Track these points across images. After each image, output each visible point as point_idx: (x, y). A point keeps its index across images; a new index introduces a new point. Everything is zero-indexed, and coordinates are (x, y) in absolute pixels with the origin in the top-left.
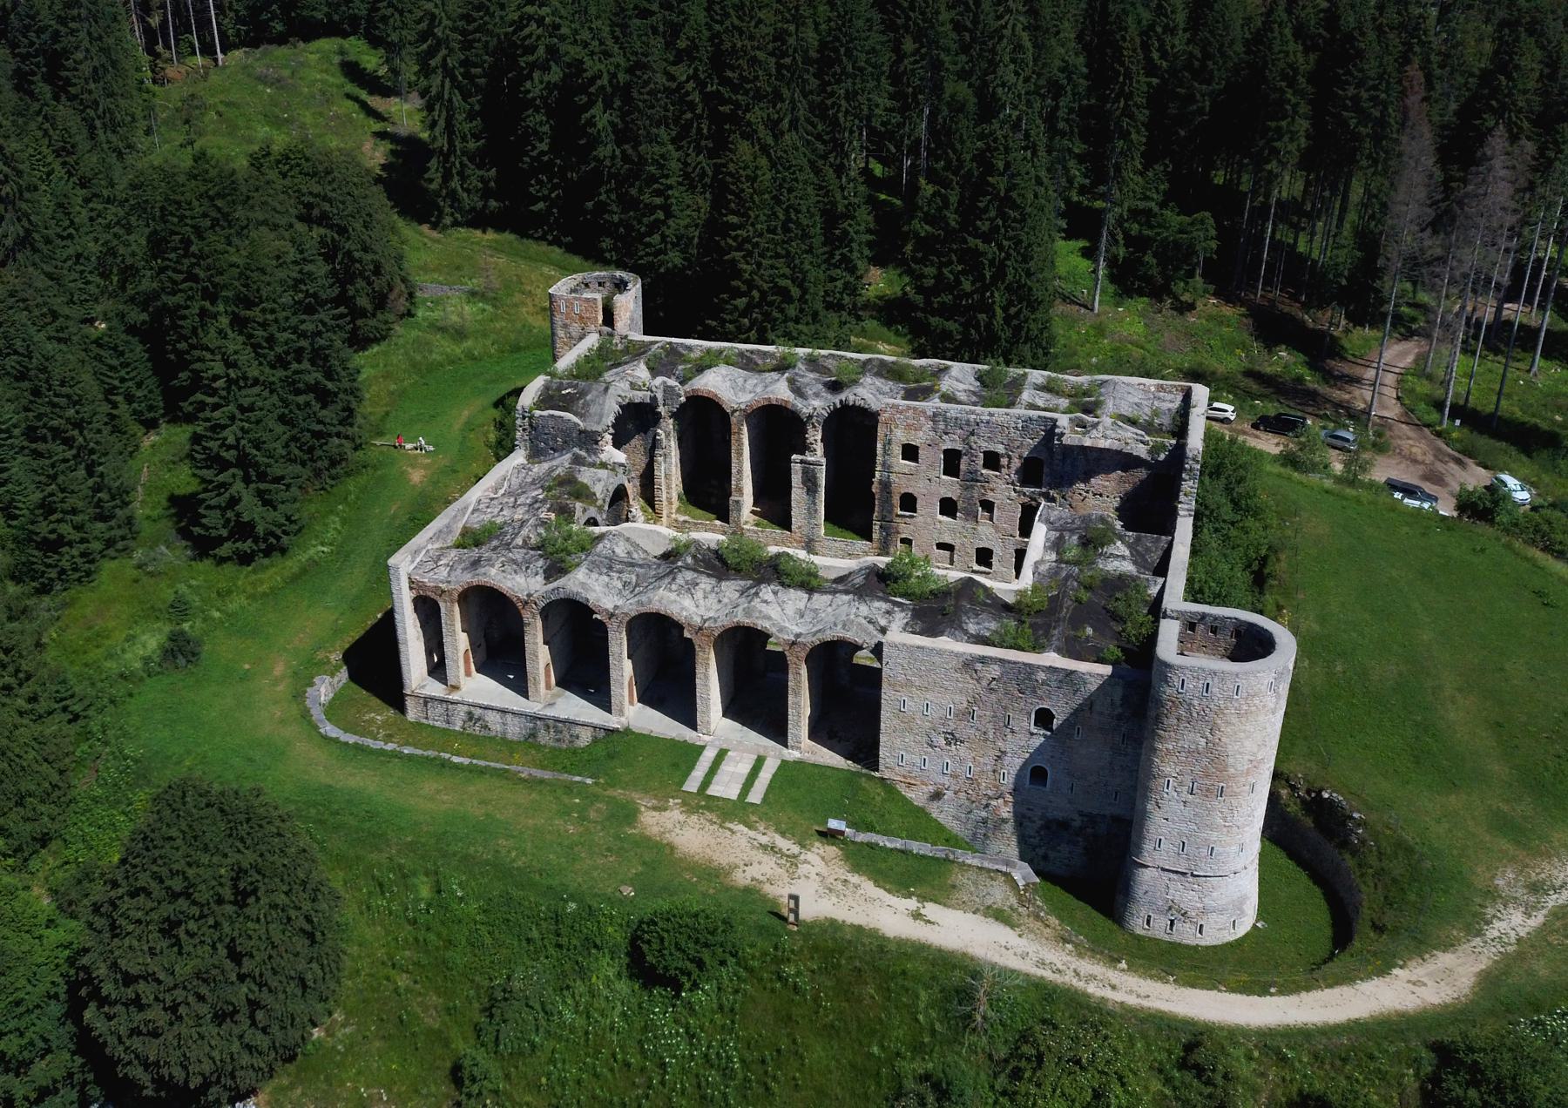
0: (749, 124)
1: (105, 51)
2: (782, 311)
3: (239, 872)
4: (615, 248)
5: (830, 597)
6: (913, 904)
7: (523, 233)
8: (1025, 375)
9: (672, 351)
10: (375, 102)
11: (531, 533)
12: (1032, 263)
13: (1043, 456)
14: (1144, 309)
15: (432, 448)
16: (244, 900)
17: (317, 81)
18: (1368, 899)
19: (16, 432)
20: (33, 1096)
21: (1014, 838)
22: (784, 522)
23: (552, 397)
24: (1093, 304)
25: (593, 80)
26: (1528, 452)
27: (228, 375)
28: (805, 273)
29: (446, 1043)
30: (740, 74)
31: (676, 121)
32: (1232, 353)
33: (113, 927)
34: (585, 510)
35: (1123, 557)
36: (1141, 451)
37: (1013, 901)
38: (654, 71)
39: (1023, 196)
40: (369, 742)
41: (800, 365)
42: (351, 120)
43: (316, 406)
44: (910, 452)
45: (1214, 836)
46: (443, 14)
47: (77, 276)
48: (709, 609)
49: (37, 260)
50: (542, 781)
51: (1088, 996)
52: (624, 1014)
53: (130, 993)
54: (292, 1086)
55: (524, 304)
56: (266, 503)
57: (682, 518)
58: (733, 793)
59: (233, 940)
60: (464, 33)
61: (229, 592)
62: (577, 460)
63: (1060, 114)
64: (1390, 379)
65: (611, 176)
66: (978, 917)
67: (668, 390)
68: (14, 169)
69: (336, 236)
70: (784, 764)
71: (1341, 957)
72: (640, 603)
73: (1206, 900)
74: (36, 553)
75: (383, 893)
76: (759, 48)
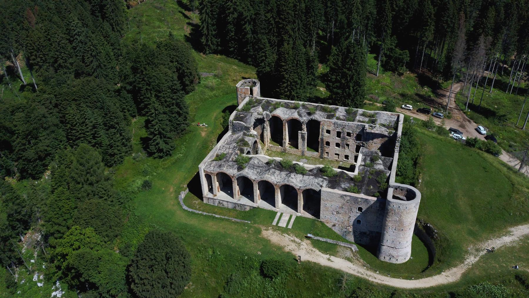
0: (287, 30)
1: (115, 5)
2: (296, 87)
3: (167, 253)
4: (252, 61)
6: (328, 256)
8: (357, 110)
9: (268, 102)
10: (186, 13)
11: (234, 157)
13: (362, 134)
18: (437, 252)
19: (101, 124)
22: (297, 147)
23: (237, 117)
25: (246, 18)
26: (487, 117)
28: (301, 77)
29: (217, 291)
32: (412, 88)
33: (137, 266)
35: (381, 164)
36: (386, 134)
37: (352, 255)
38: (262, 15)
42: (180, 19)
43: (177, 116)
44: (328, 132)
47: (112, 72)
50: (238, 222)
51: (369, 281)
52: (259, 284)
53: (142, 282)
55: (229, 79)
56: (166, 143)
57: (271, 145)
61: (158, 167)
62: (245, 134)
63: (369, 25)
64: (453, 95)
65: (250, 42)
66: (344, 260)
67: (267, 115)
70: (297, 218)
71: (430, 268)
72: (261, 178)
73: (398, 254)
74: (108, 157)
76: (289, 10)
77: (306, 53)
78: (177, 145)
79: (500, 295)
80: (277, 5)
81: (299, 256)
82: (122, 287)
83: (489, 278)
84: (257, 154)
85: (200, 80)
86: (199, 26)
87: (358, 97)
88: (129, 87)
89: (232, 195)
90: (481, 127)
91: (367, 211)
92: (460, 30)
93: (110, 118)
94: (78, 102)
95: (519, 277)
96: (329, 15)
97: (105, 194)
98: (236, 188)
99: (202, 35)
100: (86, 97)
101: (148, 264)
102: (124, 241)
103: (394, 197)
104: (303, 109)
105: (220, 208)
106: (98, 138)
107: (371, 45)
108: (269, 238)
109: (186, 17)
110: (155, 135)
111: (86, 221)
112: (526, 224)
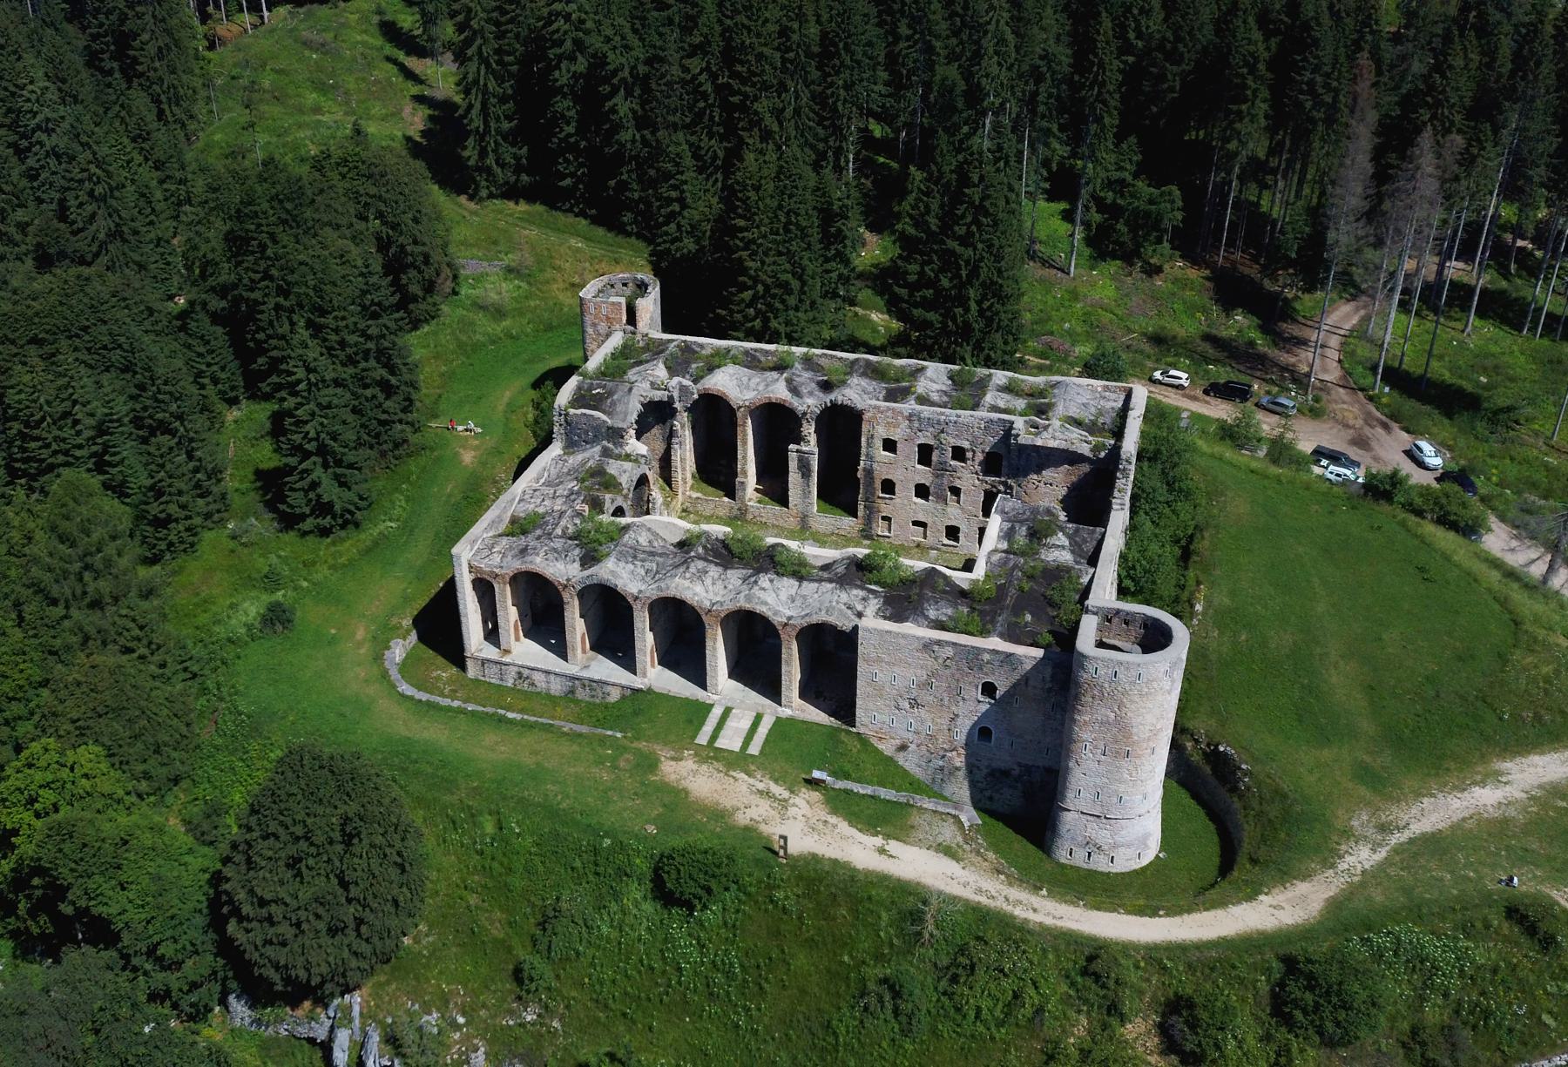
0: (756, 113)
1: (168, 32)
2: (783, 302)
3: (346, 820)
4: (635, 222)
5: (817, 585)
6: (878, 841)
7: (552, 204)
8: (990, 375)
9: (687, 349)
10: (412, 63)
11: (569, 524)
12: (1003, 263)
13: (1002, 451)
14: (1116, 273)
15: (480, 430)
16: (350, 840)
17: (358, 42)
18: (1249, 834)
19: (126, 420)
20: (186, 988)
21: (966, 783)
22: (784, 501)
23: (583, 396)
24: (1069, 269)
25: (615, 72)
27: (309, 379)
29: (509, 949)
30: (748, 69)
31: (690, 109)
32: (1193, 316)
33: (249, 861)
34: (613, 501)
35: (1063, 547)
36: (1085, 449)
37: (960, 839)
38: (670, 64)
39: (996, 205)
40: (439, 699)
41: (797, 365)
42: (391, 84)
43: (381, 396)
44: (890, 445)
45: (1122, 788)
46: (478, 8)
47: (158, 257)
48: (716, 594)
49: (127, 250)
50: (580, 735)
51: (1013, 917)
52: (649, 928)
54: (388, 983)
57: (695, 495)
58: (736, 746)
59: (342, 872)
60: (497, 24)
61: (314, 563)
62: (606, 453)
63: (1040, 98)
64: (1334, 341)
66: (932, 853)
68: (104, 171)
69: (390, 232)
70: (779, 722)
72: (659, 589)
74: (148, 528)
75: (456, 829)
76: (766, 45)
77: (818, 189)
78: (380, 494)
79: (1453, 967)
80: (724, 31)
81: (781, 837)
82: (198, 937)
83: (1416, 912)
84: (648, 513)
85: (457, 284)
86: (455, 107)
87: (997, 337)
88: (217, 304)
89: (561, 651)
90: (1424, 445)
91: (1012, 696)
92: (1358, 114)
93: (157, 400)
94: (48, 349)
95: (1517, 911)
96: (903, 65)
97: (139, 640)
98: (577, 626)
99: (467, 134)
100: (74, 331)
101: (283, 854)
102: (200, 796)
103: (1101, 644)
104: (807, 370)
105: (524, 692)
106: (115, 466)
107: (1049, 171)
108: (684, 784)
109: (409, 75)
110: (307, 455)
111: (80, 723)
112: (1556, 750)
